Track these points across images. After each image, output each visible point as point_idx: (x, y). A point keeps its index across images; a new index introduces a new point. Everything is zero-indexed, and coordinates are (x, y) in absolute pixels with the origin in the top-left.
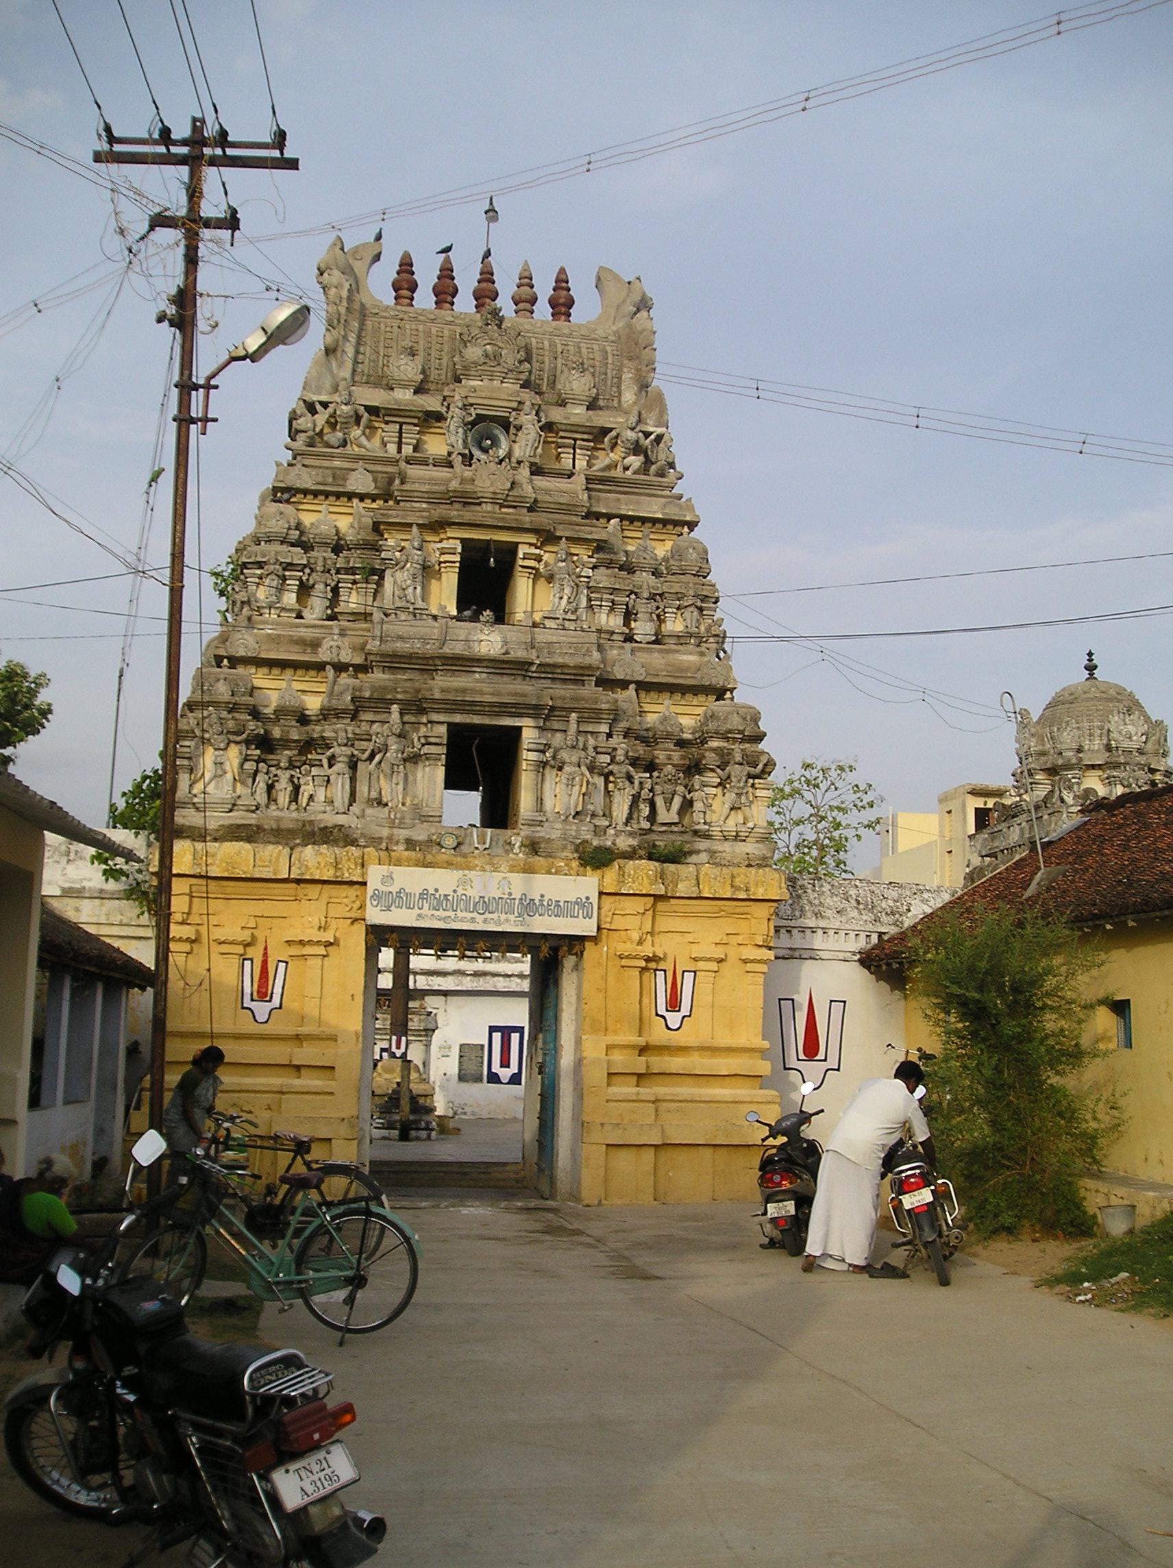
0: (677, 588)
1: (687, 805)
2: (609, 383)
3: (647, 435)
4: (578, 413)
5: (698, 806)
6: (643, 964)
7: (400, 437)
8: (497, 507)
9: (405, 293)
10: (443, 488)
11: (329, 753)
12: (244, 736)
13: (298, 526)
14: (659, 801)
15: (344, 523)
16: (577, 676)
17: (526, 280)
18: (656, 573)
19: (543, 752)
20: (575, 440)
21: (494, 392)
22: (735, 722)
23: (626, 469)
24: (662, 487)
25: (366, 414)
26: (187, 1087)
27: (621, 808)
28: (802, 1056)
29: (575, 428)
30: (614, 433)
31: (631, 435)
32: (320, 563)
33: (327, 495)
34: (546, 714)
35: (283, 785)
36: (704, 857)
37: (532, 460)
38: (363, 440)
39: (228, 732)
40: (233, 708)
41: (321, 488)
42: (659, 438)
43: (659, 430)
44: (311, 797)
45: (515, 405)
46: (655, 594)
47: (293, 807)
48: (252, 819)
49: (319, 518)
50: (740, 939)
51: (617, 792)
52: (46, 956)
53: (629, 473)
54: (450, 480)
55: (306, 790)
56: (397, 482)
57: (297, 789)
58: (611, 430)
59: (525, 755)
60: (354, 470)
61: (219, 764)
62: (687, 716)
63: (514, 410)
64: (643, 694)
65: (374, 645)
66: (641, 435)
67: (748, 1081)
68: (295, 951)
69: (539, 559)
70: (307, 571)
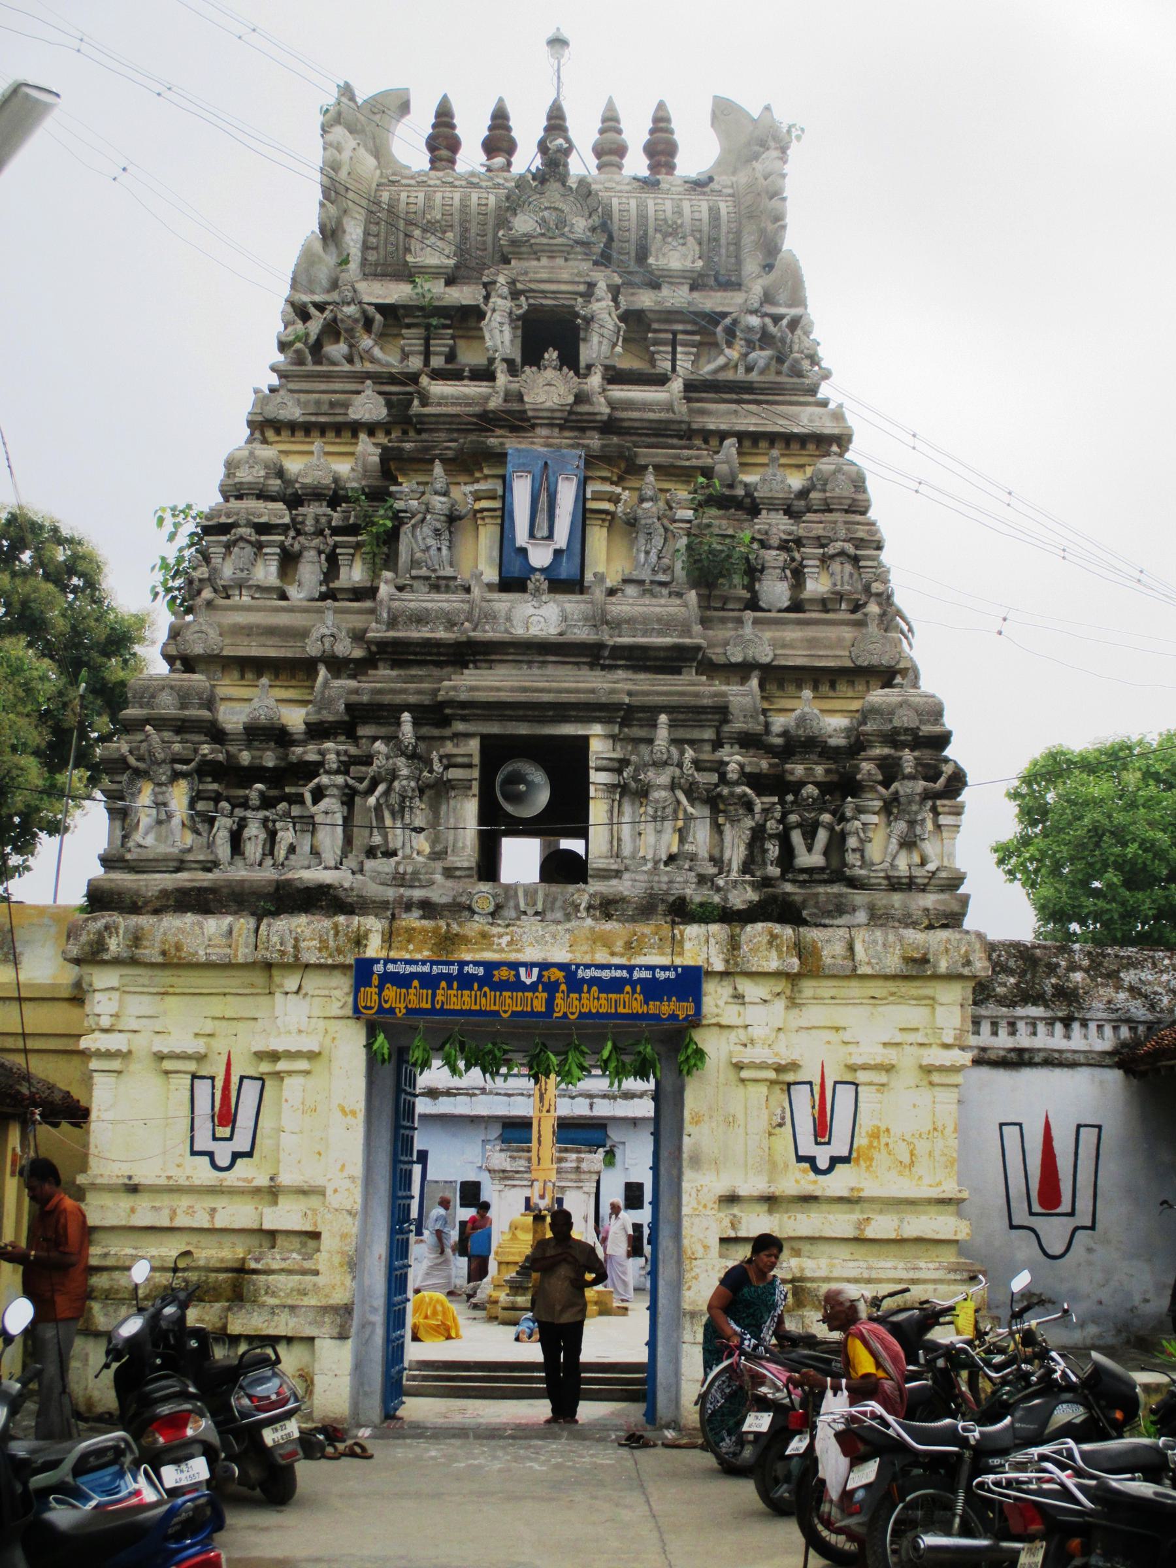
0: (818, 530)
1: (837, 842)
2: (723, 251)
3: (777, 319)
4: (676, 297)
5: (852, 842)
6: (772, 1075)
7: (427, 345)
8: (557, 430)
9: (444, 153)
10: (477, 409)
11: (312, 785)
12: (193, 764)
13: (280, 473)
14: (796, 837)
15: (343, 468)
16: (673, 660)
17: (611, 122)
18: (789, 512)
19: (619, 771)
20: (675, 333)
22: (905, 719)
23: (749, 369)
24: (795, 390)
25: (378, 317)
27: (735, 852)
28: (1037, 1208)
29: (670, 315)
30: (728, 321)
31: (754, 321)
32: (310, 522)
33: (323, 429)
34: (629, 718)
35: (254, 830)
36: (861, 917)
37: (607, 362)
38: (377, 352)
39: (175, 761)
40: (182, 727)
41: (313, 419)
42: (794, 324)
43: (793, 312)
44: (292, 849)
45: (582, 288)
46: (787, 541)
47: (269, 861)
48: (204, 879)
49: (311, 463)
50: (919, 1038)
51: (728, 826)
53: (754, 373)
54: (487, 398)
55: (286, 836)
56: (416, 402)
57: (272, 835)
58: (724, 315)
59: (596, 777)
60: (358, 393)
61: (160, 804)
62: (833, 721)
63: (581, 295)
64: (772, 688)
65: (377, 632)
66: (768, 320)
67: (893, 1249)
68: (265, 1067)
69: (615, 499)
70: (292, 533)
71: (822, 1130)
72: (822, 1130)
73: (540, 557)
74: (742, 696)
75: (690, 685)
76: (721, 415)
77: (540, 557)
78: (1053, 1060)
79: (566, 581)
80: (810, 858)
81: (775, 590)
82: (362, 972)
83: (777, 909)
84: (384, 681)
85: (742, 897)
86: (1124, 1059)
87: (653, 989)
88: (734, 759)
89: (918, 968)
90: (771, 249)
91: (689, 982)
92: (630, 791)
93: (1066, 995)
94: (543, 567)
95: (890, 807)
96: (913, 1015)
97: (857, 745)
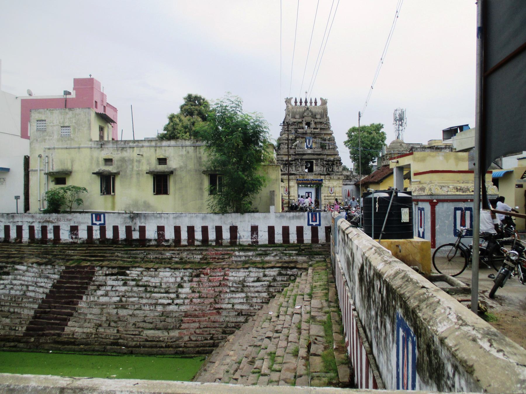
4: (318, 120)
21: (308, 119)
26: (224, 284)
27: (325, 170)
34: (317, 160)
52: (162, 192)
62: (332, 158)
71: (331, 191)
72: (331, 191)
73: (309, 146)
74: (325, 157)
75: (321, 157)
76: (323, 132)
77: (309, 146)
78: (349, 185)
79: (311, 148)
80: (330, 170)
81: (327, 148)
82: (297, 180)
83: (328, 174)
84: (297, 157)
85: (325, 173)
86: (355, 184)
87: (319, 181)
88: (325, 163)
89: (339, 179)
90: (326, 115)
91: (322, 180)
92: (317, 165)
93: (350, 179)
94: (308, 147)
95: (337, 166)
96: (338, 182)
97: (334, 161)
